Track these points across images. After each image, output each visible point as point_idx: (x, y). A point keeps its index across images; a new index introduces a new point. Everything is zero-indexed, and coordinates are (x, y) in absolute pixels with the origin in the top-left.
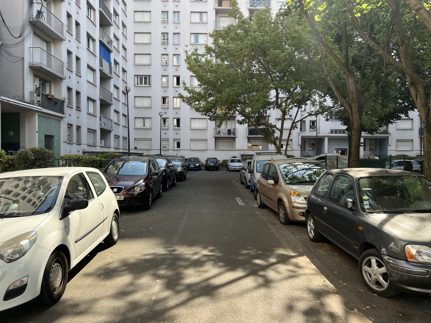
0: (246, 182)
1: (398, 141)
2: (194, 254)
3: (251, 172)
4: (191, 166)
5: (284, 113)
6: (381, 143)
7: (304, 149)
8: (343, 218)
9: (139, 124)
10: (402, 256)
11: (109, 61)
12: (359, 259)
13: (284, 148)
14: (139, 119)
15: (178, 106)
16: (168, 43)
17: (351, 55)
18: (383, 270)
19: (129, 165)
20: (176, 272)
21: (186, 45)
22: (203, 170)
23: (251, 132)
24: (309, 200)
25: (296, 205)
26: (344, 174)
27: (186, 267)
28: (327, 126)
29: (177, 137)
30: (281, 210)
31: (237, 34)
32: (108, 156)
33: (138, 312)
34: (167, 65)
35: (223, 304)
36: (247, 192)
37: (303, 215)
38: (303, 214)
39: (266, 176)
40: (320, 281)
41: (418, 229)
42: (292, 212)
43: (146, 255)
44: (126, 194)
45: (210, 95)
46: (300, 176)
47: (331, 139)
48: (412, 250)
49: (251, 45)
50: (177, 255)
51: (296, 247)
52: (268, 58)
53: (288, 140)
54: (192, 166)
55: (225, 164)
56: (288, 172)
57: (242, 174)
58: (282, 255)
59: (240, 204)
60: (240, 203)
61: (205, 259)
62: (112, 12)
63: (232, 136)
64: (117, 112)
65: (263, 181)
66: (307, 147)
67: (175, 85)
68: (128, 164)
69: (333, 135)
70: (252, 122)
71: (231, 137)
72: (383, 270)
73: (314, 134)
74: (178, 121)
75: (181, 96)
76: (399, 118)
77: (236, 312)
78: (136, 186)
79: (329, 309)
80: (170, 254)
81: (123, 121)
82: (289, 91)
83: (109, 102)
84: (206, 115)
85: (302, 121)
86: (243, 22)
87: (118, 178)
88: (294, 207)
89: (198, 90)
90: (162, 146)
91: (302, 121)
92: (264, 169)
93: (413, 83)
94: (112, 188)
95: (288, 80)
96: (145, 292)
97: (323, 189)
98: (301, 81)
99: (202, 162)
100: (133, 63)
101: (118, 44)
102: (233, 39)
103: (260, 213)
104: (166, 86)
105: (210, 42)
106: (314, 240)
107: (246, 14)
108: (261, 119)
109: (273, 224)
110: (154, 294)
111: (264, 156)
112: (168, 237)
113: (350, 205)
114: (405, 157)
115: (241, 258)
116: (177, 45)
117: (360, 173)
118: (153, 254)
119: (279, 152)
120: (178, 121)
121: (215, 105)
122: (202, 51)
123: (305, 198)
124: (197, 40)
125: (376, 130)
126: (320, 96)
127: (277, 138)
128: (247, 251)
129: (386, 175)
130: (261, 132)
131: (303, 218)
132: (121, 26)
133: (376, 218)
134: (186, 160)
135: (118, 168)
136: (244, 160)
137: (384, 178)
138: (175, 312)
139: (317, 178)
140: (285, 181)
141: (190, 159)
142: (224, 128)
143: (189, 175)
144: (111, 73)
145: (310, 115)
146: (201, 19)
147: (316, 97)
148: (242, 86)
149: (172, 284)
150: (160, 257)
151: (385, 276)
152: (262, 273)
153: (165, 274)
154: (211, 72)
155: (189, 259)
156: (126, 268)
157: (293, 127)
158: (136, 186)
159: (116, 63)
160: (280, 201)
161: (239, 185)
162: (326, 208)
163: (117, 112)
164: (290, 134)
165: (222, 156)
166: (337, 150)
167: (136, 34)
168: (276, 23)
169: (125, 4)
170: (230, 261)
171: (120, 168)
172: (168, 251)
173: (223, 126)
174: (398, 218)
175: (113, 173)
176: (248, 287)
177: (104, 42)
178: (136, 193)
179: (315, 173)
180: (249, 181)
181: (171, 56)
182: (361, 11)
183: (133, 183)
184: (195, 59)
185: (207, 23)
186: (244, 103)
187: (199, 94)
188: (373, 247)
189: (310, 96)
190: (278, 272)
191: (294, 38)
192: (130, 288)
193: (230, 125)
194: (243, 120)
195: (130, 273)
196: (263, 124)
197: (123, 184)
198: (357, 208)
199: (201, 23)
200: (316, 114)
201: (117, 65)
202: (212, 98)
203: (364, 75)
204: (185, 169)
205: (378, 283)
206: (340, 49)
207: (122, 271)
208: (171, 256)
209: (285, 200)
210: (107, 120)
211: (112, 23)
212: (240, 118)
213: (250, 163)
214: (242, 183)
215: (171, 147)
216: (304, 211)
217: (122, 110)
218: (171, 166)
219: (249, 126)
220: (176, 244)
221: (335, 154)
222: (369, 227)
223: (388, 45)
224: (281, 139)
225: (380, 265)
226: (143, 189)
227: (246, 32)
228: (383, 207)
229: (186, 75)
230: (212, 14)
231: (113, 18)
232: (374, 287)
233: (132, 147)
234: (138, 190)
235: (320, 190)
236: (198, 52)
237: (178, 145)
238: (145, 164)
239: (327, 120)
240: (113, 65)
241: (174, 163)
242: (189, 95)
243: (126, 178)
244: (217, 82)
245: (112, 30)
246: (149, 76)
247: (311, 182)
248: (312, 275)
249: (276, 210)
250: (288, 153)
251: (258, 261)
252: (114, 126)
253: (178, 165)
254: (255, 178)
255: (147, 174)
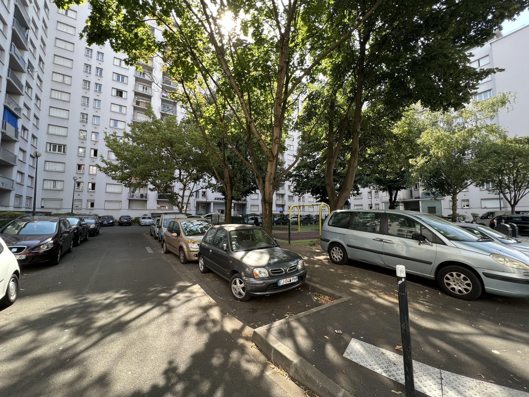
0: (155, 235)
1: (251, 205)
2: (106, 299)
3: (160, 227)
4: (104, 223)
5: (185, 186)
6: (243, 206)
7: (198, 209)
8: (222, 256)
9: (49, 185)
10: (252, 275)
11: (15, 125)
12: (230, 281)
13: (185, 209)
14: (49, 182)
15: (94, 172)
16: (87, 121)
17: (226, 155)
18: (243, 285)
19: (34, 225)
20: (87, 318)
21: (105, 127)
22: (116, 226)
23: (160, 197)
24: (201, 246)
25: (192, 249)
26: (222, 229)
27: (98, 312)
28: (213, 196)
29: (91, 198)
30: (182, 254)
31: (151, 128)
32: (5, 215)
33: (40, 367)
34: (85, 138)
35: (133, 335)
36: (156, 242)
37: (196, 256)
38: (197, 256)
39: (171, 230)
40: (207, 300)
41: (260, 259)
42: (189, 255)
43: (53, 309)
44: (28, 253)
45: (126, 168)
46: (194, 230)
47: (215, 204)
48: (257, 271)
49: (162, 138)
50: (88, 303)
51: (191, 279)
52: (174, 149)
53: (187, 203)
54: (105, 222)
55: (137, 221)
56: (187, 227)
57: (152, 229)
58: (182, 286)
59: (149, 252)
60: (149, 250)
61: (117, 301)
62: (24, 84)
63: (144, 199)
64: (21, 173)
65: (169, 234)
66: (200, 208)
67: (92, 156)
68: (33, 224)
69: (217, 201)
70: (161, 190)
71: (143, 200)
72: (243, 285)
73: (204, 200)
74: (93, 185)
75: (98, 167)
76: (252, 193)
77: (145, 338)
78: (43, 245)
79: (212, 317)
80: (80, 303)
81: (27, 182)
82: (188, 172)
83: (11, 163)
84: (121, 183)
85: (197, 191)
86: (156, 121)
87: (17, 238)
88: (190, 251)
89: (116, 163)
90: (74, 206)
91: (197, 191)
92: (170, 225)
93: (257, 177)
94: (11, 249)
95: (188, 164)
96: (51, 344)
97: (209, 238)
98: (196, 166)
99: (115, 219)
100: (46, 132)
101: (29, 113)
102: (148, 131)
103: (165, 257)
104: (83, 155)
105: (128, 130)
106: (204, 272)
107: (158, 117)
108: (168, 188)
109: (175, 264)
110: (61, 344)
111: (169, 215)
112: (77, 288)
113: (225, 248)
114: (255, 215)
115: (149, 294)
116: (96, 126)
117: (231, 227)
118: (62, 306)
119: (181, 213)
120: (93, 185)
121: (130, 176)
122: (120, 134)
123: (198, 245)
124: (116, 125)
125: (240, 200)
126: (208, 177)
127: (179, 202)
128: (154, 288)
129: (244, 228)
130: (167, 196)
131: (196, 258)
132: (34, 97)
133: (239, 255)
134: (100, 217)
135: (20, 228)
136: (154, 217)
137: (243, 230)
138: (86, 354)
139: (206, 231)
140: (185, 233)
141: (104, 217)
142: (138, 192)
143: (102, 230)
144: (16, 136)
145: (202, 188)
146: (121, 110)
147: (206, 177)
148: (154, 165)
149: (81, 331)
150: (69, 308)
151: (243, 289)
152: (166, 303)
153: (74, 323)
154: (127, 151)
155: (101, 304)
156: (26, 326)
157: (191, 195)
158: (43, 245)
159: (24, 129)
160: (181, 248)
161: (149, 237)
162: (211, 251)
163: (21, 173)
164: (189, 200)
165: (134, 214)
166: (219, 210)
167: (52, 109)
168: (180, 127)
169: (41, 81)
170: (139, 299)
171: (22, 228)
172: (78, 301)
173: (137, 191)
174: (251, 253)
175: (13, 233)
176: (155, 316)
177: (10, 108)
178: (41, 251)
179: (205, 227)
180: (158, 234)
181: (89, 132)
182: (232, 132)
183: (39, 241)
184: (113, 140)
185: (125, 114)
186: (155, 176)
187: (116, 166)
188: (237, 272)
189: (202, 176)
190: (178, 300)
191: (192, 139)
192: (33, 345)
193: (142, 191)
194: (154, 188)
195: (32, 330)
196: (169, 192)
197: (24, 243)
198: (229, 250)
199: (120, 113)
200: (206, 188)
201: (26, 131)
202: (128, 170)
203: (233, 167)
204: (98, 226)
205: (240, 294)
206: (221, 150)
207: (21, 331)
208: (82, 305)
209: (185, 247)
210: (7, 180)
211: (23, 93)
212: (151, 186)
213: (158, 220)
214: (152, 235)
215: (84, 206)
216: (197, 253)
217: (26, 170)
218: (84, 224)
219: (158, 192)
220: (88, 293)
221: (217, 213)
222: (235, 260)
223: (246, 153)
224: (182, 203)
225: (241, 283)
226: (51, 247)
227: (158, 128)
228: (242, 247)
229: (104, 150)
230: (130, 110)
231: (25, 89)
232: (238, 297)
233: (38, 205)
234: (44, 248)
235: (208, 239)
236: (117, 135)
237: (92, 205)
238: (55, 224)
239: (213, 192)
240: (20, 130)
241: (86, 221)
242: (106, 166)
243: (28, 237)
244: (133, 159)
245: (22, 100)
246: (64, 146)
247: (203, 233)
248: (201, 296)
249: (178, 254)
250: (187, 212)
251: (163, 295)
252: (16, 186)
253: (91, 223)
254: (162, 231)
255: (57, 233)
